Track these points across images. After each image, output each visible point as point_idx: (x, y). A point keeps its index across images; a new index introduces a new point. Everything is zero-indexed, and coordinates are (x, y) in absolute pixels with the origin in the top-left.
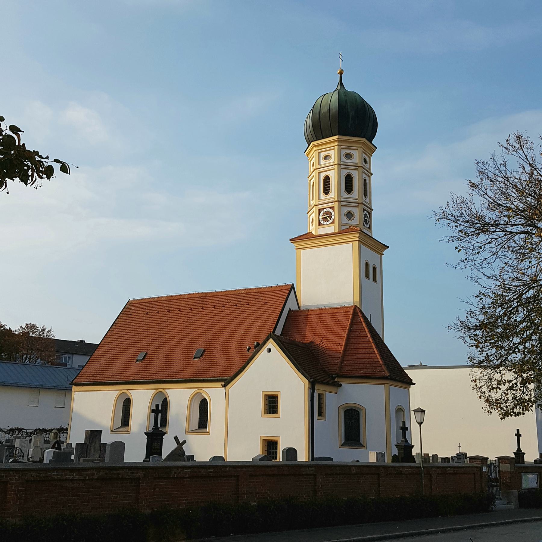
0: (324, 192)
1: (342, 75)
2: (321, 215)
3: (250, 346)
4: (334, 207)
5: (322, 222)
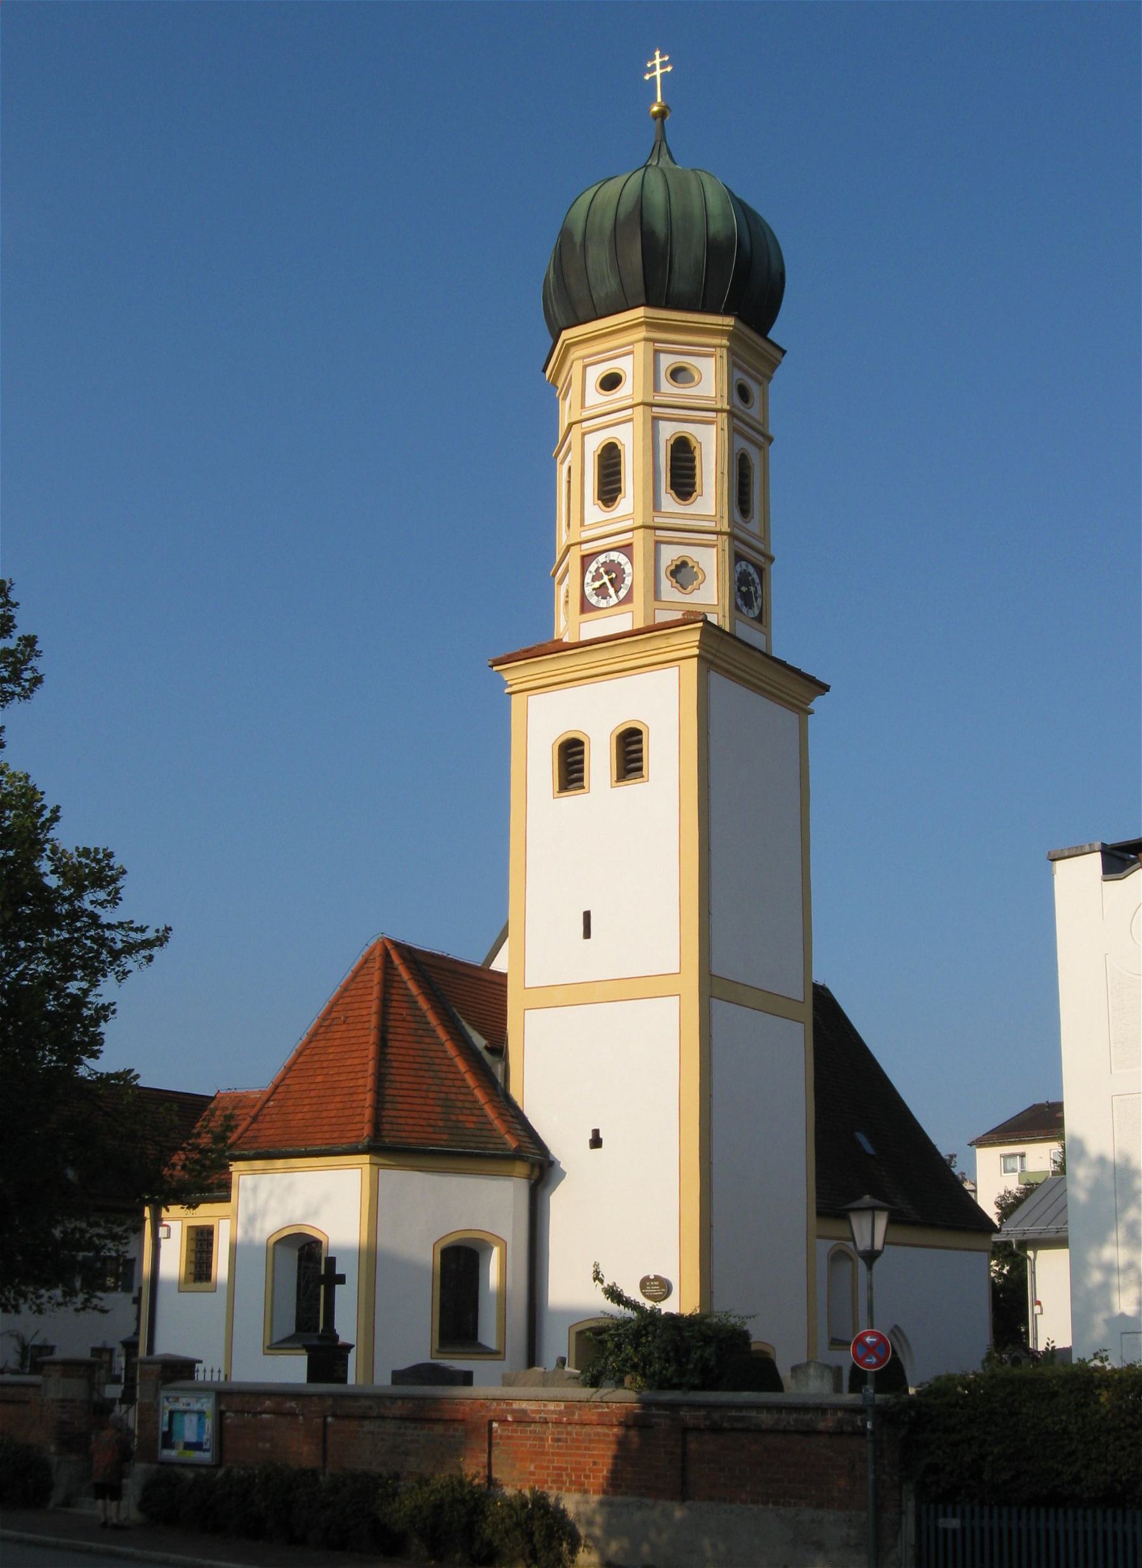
2: (588, 577)
4: (630, 545)
5: (594, 600)
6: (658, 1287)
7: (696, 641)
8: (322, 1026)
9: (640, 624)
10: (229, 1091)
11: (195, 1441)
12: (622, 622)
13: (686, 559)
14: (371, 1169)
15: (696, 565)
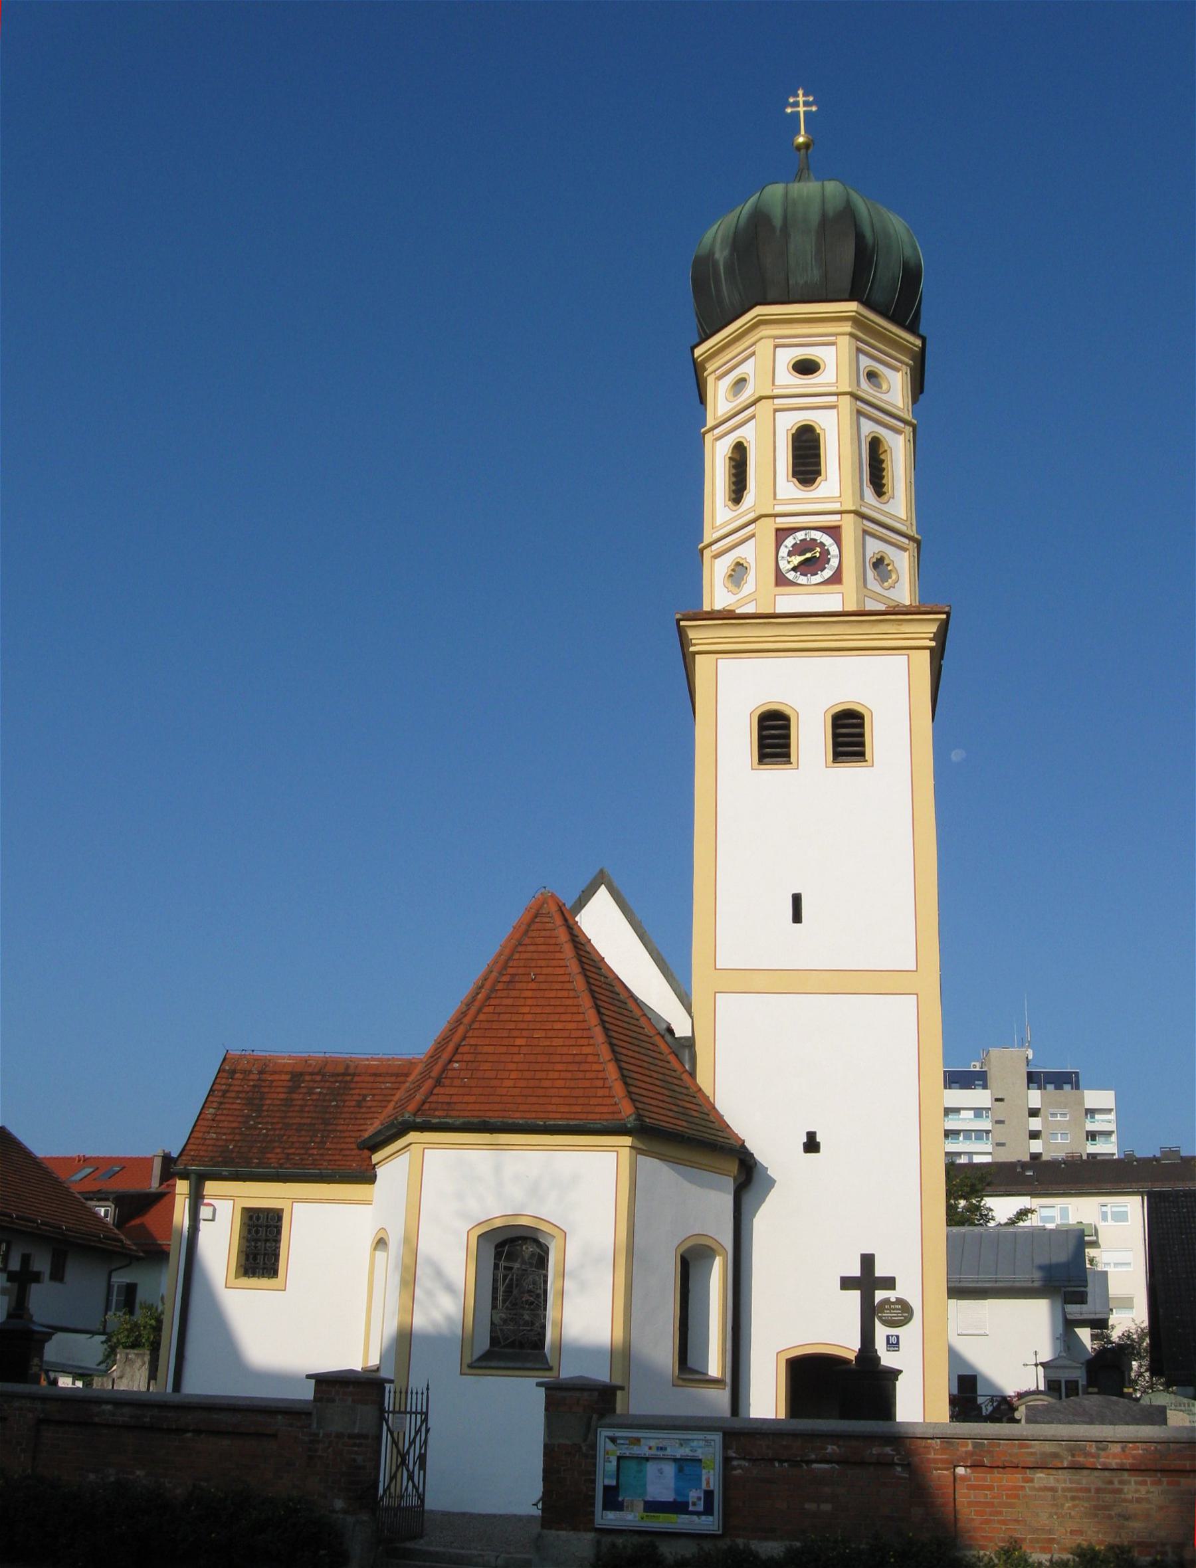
2: (783, 551)
6: (900, 1312)
7: (931, 633)
8: (499, 982)
9: (852, 607)
10: (244, 1053)
11: (671, 1500)
12: (831, 601)
13: (885, 555)
14: (630, 1151)
15: (892, 563)
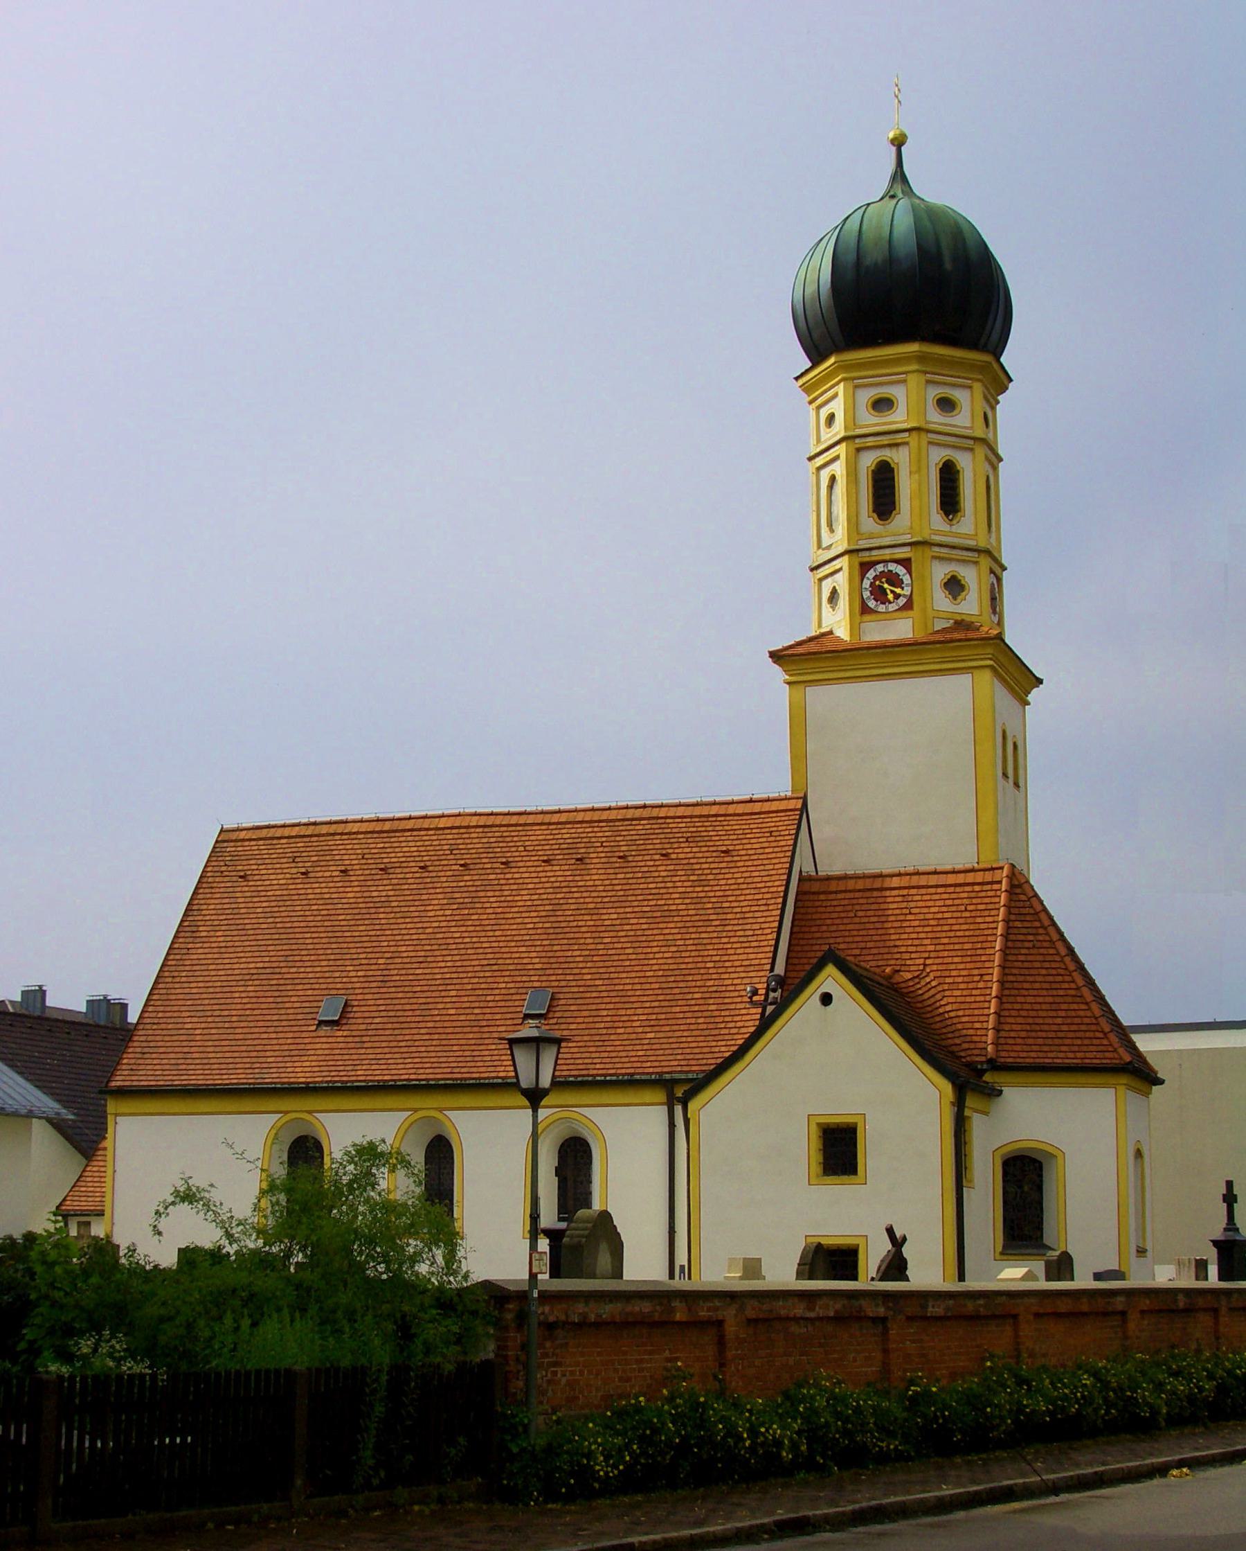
0: (874, 511)
1: (903, 148)
3: (757, 986)
